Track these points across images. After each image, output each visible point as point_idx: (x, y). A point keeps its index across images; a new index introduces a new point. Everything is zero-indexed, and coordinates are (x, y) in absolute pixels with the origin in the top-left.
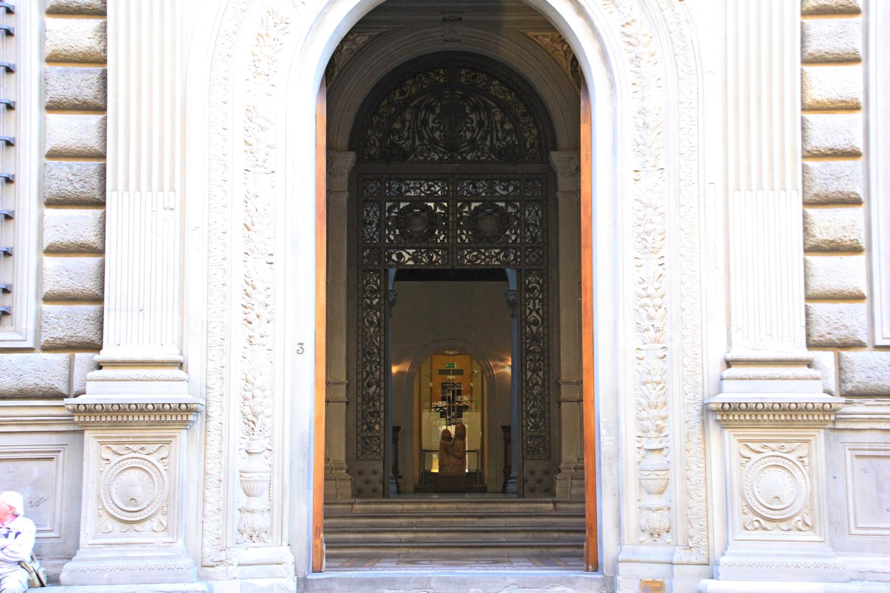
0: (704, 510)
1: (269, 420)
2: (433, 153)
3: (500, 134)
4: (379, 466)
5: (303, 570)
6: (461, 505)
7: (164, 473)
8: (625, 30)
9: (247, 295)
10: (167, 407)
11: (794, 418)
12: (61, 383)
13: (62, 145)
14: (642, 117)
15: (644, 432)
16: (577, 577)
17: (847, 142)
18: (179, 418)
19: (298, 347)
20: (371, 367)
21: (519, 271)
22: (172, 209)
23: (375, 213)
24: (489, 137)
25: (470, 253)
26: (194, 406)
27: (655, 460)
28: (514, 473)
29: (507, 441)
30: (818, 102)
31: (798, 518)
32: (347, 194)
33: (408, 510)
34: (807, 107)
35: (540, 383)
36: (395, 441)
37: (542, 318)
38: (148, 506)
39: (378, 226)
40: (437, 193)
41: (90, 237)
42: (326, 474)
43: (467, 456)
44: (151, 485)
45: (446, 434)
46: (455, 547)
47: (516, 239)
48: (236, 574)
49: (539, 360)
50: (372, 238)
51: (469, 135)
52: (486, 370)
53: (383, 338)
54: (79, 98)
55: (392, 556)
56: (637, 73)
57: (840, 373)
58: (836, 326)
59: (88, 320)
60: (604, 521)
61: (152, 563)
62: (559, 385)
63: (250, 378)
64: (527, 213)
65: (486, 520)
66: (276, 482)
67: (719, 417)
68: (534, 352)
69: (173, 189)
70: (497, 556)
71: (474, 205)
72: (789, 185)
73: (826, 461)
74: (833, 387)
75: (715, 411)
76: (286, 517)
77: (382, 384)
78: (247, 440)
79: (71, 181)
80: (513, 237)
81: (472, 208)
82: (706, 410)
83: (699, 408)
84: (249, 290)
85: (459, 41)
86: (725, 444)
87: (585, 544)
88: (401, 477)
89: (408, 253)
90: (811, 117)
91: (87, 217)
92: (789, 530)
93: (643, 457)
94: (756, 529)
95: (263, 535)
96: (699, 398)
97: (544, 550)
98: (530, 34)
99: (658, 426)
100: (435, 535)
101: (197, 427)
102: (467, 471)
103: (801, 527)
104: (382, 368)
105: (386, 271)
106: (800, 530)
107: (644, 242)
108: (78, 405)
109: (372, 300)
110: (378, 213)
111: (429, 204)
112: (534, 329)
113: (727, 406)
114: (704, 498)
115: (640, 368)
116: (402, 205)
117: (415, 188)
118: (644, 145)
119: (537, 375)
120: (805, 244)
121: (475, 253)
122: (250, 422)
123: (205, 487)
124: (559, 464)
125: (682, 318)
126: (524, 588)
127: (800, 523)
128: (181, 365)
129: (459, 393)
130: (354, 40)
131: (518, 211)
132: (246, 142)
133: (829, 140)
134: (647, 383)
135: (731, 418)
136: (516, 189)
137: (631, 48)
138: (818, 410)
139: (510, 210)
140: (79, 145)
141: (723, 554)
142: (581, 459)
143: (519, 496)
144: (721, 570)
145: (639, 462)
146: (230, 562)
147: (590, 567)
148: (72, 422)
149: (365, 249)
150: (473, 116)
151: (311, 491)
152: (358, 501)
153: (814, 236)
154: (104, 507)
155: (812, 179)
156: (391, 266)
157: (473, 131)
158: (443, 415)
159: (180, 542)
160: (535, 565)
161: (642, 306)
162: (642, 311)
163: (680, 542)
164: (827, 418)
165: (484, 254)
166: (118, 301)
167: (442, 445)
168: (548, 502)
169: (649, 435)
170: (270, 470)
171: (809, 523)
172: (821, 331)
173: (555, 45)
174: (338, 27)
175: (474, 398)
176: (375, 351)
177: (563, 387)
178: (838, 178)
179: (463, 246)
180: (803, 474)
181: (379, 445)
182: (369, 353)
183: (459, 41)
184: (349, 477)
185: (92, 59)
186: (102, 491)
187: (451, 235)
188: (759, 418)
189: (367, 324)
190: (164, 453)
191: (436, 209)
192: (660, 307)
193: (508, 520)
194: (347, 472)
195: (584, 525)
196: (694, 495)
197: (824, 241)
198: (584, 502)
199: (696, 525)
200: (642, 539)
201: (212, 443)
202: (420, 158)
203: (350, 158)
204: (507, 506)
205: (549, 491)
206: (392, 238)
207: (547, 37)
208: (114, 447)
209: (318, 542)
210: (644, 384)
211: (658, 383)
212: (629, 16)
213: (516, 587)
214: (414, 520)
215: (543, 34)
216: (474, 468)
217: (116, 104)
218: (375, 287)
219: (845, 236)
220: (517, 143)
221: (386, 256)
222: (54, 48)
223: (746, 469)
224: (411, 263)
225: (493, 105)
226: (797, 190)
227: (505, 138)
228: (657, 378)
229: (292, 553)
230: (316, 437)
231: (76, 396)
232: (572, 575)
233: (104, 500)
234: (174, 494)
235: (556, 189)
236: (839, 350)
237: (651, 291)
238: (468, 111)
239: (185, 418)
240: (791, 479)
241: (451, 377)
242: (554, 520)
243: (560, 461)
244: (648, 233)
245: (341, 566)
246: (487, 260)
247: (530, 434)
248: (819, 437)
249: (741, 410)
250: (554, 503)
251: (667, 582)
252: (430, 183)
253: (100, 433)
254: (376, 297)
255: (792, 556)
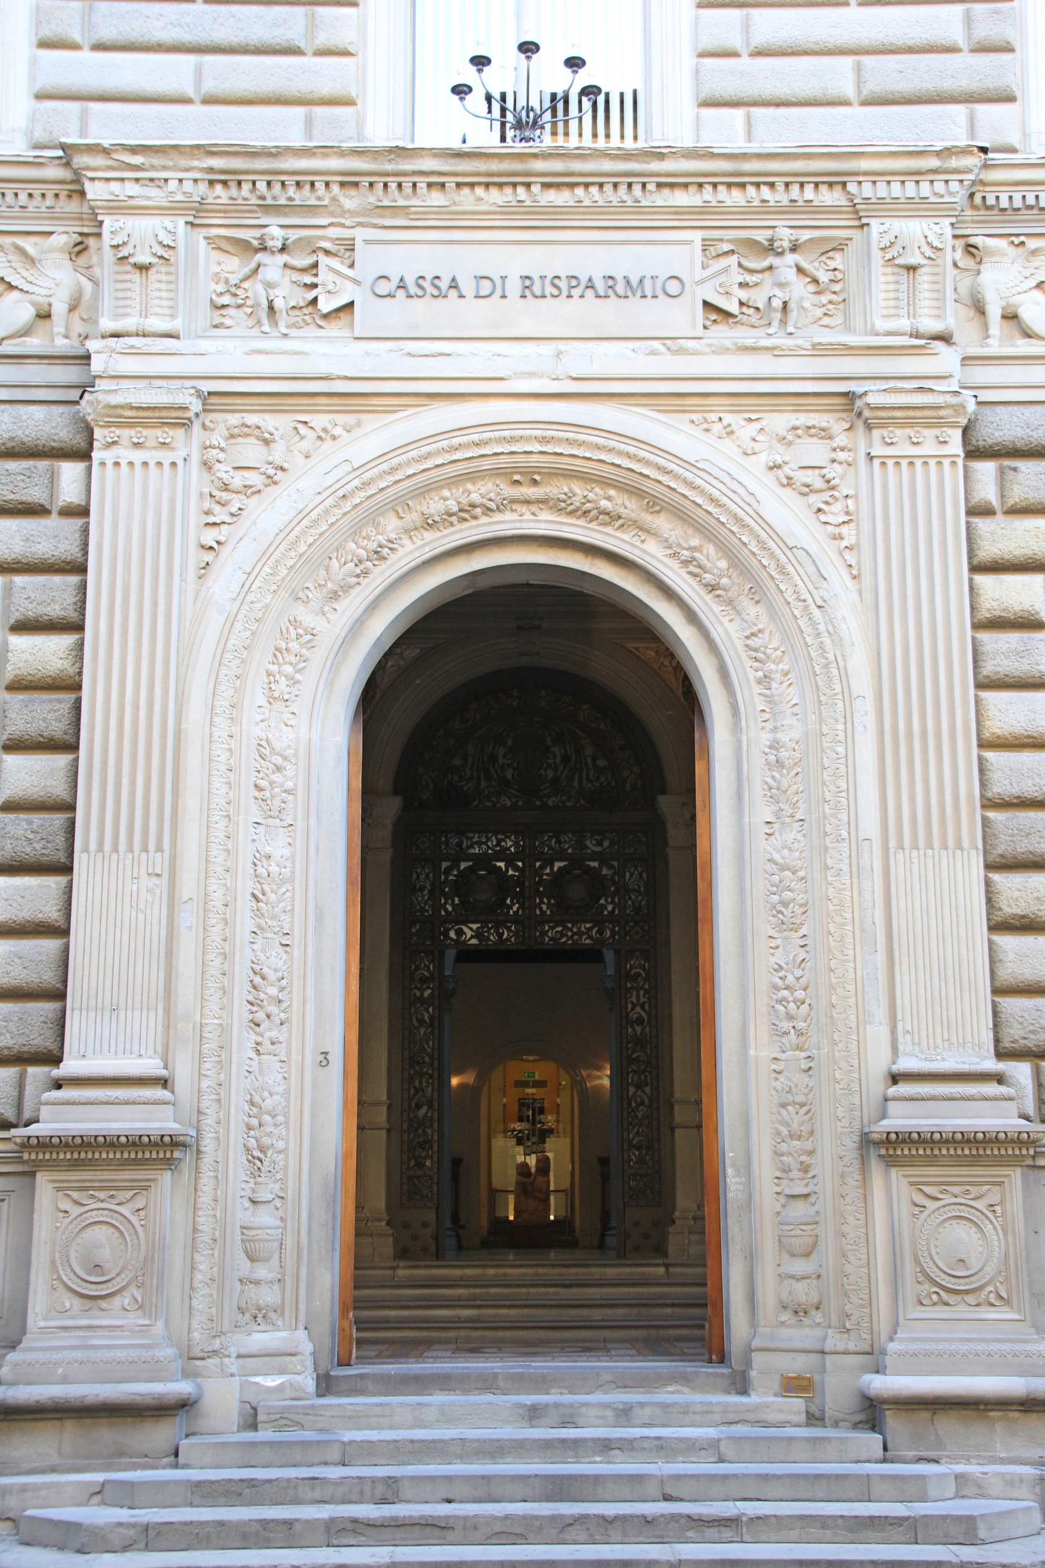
0: (866, 1277)
1: (282, 1156)
2: (503, 798)
3: (591, 773)
4: (431, 1217)
5: (325, 1364)
6: (541, 1270)
7: (140, 1229)
8: (749, 642)
9: (254, 987)
10: (146, 1139)
11: (981, 1152)
12: (7, 1107)
13: (21, 794)
14: (775, 752)
15: (784, 1171)
16: (696, 1372)
17: (1037, 788)
18: (161, 1156)
19: (321, 1058)
20: (421, 1083)
21: (617, 952)
22: (158, 875)
23: (427, 876)
24: (577, 779)
25: (552, 928)
26: (181, 1138)
27: (799, 1210)
28: (613, 1223)
29: (605, 1177)
30: (999, 737)
31: (990, 1288)
32: (391, 850)
33: (470, 1276)
34: (985, 743)
35: (647, 1102)
36: (456, 1178)
37: (649, 1014)
38: (118, 1275)
39: (431, 893)
40: (509, 849)
41: (51, 913)
42: (357, 1229)
43: (552, 1198)
44: (122, 1247)
45: (523, 1169)
46: (533, 1328)
47: (613, 910)
48: (234, 1369)
49: (645, 1071)
50: (423, 909)
51: (550, 774)
52: (579, 1085)
53: (436, 1044)
54: (45, 734)
55: (447, 1341)
56: (765, 696)
57: (1039, 1091)
58: (1032, 1028)
59: (45, 1022)
60: (731, 1290)
61: (121, 1355)
62: (672, 1106)
63: (257, 1099)
64: (628, 875)
65: (574, 1290)
66: (289, 1242)
67: (883, 1152)
68: (637, 1060)
69: (159, 849)
70: (590, 1341)
71: (558, 865)
72: (966, 843)
73: (1025, 1210)
74: (1031, 1111)
75: (878, 1144)
76: (302, 1291)
77: (436, 1104)
78: (252, 1185)
79: (30, 840)
80: (610, 908)
81: (556, 869)
82: (866, 1142)
83: (857, 1139)
84: (257, 980)
85: (538, 654)
86: (892, 1189)
87: (707, 1326)
88: (463, 1227)
89: (471, 929)
90: (990, 755)
91: (49, 886)
92: (977, 1305)
93: (784, 1206)
94: (935, 1304)
95: (272, 1315)
96: (857, 1125)
97: (653, 1332)
98: (630, 646)
99: (802, 1163)
100: (505, 1311)
101: (185, 1168)
102: (552, 1217)
103: (993, 1301)
104: (436, 1084)
105: (442, 953)
106: (993, 1305)
107: (780, 916)
108: (29, 1137)
109: (422, 991)
110: (431, 875)
111: (499, 864)
112: (639, 1029)
113: (893, 1136)
114: (864, 1262)
115: (777, 1084)
116: (463, 865)
117: (480, 844)
118: (778, 789)
119: (643, 1091)
120: (989, 920)
121: (560, 929)
122: (256, 1159)
123: (194, 1249)
124: (673, 1213)
125: (832, 1017)
126: (625, 1387)
127: (992, 1295)
128: (164, 1083)
129: (542, 1111)
130: (401, 653)
131: (615, 874)
132: (256, 786)
133: (1015, 785)
134: (788, 1104)
135: (899, 1152)
136: (612, 844)
137: (756, 664)
138: (1012, 1141)
139: (605, 871)
140: (42, 794)
141: (891, 1339)
142: (700, 1206)
143: (619, 1257)
144: (888, 1360)
145: (778, 1213)
146: (227, 1353)
147: (714, 1357)
148: (20, 1160)
149: (413, 923)
150: (556, 749)
151: (337, 1254)
152: (402, 1264)
153: (1000, 909)
154: (59, 1278)
155: (994, 835)
156: (449, 946)
157: (556, 769)
158: (520, 1142)
159: (160, 1325)
160: (640, 1353)
161: (780, 1001)
162: (779, 1007)
163: (834, 1321)
164: (1024, 1152)
165: (571, 930)
166: (85, 996)
167: (518, 1183)
168: (657, 1265)
169: (791, 1175)
170: (282, 1225)
171: (1005, 1295)
172: (1014, 1034)
173: (662, 660)
174: (379, 638)
175: (561, 1118)
176: (427, 1059)
177: (676, 1107)
178: (1029, 834)
179: (543, 919)
180: (995, 1228)
181: (431, 1187)
182: (418, 1063)
183: (538, 654)
184: (391, 1232)
185: (63, 684)
186: (57, 1255)
187: (527, 904)
188: (936, 1152)
189: (416, 1024)
190: (140, 1203)
191: (507, 871)
192: (803, 1003)
193: (604, 1290)
194: (388, 1224)
195: (705, 1296)
196: (852, 1259)
197: (1014, 916)
198: (704, 1265)
199: (854, 1299)
200: (783, 1318)
201: (205, 1189)
202: (487, 804)
203: (392, 807)
204: (602, 1270)
205: (659, 1250)
206: (450, 908)
207: (652, 649)
208: (75, 1195)
209: (346, 1324)
210: (784, 1105)
211: (802, 1105)
212: (755, 625)
213: (614, 1386)
214: (478, 1291)
215: (646, 645)
216: (562, 1213)
217: (91, 741)
218: (426, 974)
219: (1039, 910)
220: (613, 784)
221: (442, 933)
222: (17, 672)
223: (920, 1222)
224: (474, 941)
225: (584, 736)
226: (977, 849)
227: (598, 778)
228: (800, 1099)
229: (311, 1339)
230: (344, 1181)
231: (26, 1125)
232: (689, 1369)
233: (60, 1268)
234: (153, 1258)
235: (665, 843)
236: (1038, 1061)
237: (791, 979)
238: (549, 743)
239: (168, 1155)
240: (979, 1235)
241: (530, 1091)
242: (666, 1289)
243: (674, 1208)
244: (785, 904)
245: (378, 1356)
246: (576, 937)
247: (632, 1171)
248: (1016, 1176)
249: (912, 1142)
250: (667, 1266)
251: (817, 1378)
252: (500, 837)
253: (56, 1176)
254: (428, 988)
255: (982, 1340)
